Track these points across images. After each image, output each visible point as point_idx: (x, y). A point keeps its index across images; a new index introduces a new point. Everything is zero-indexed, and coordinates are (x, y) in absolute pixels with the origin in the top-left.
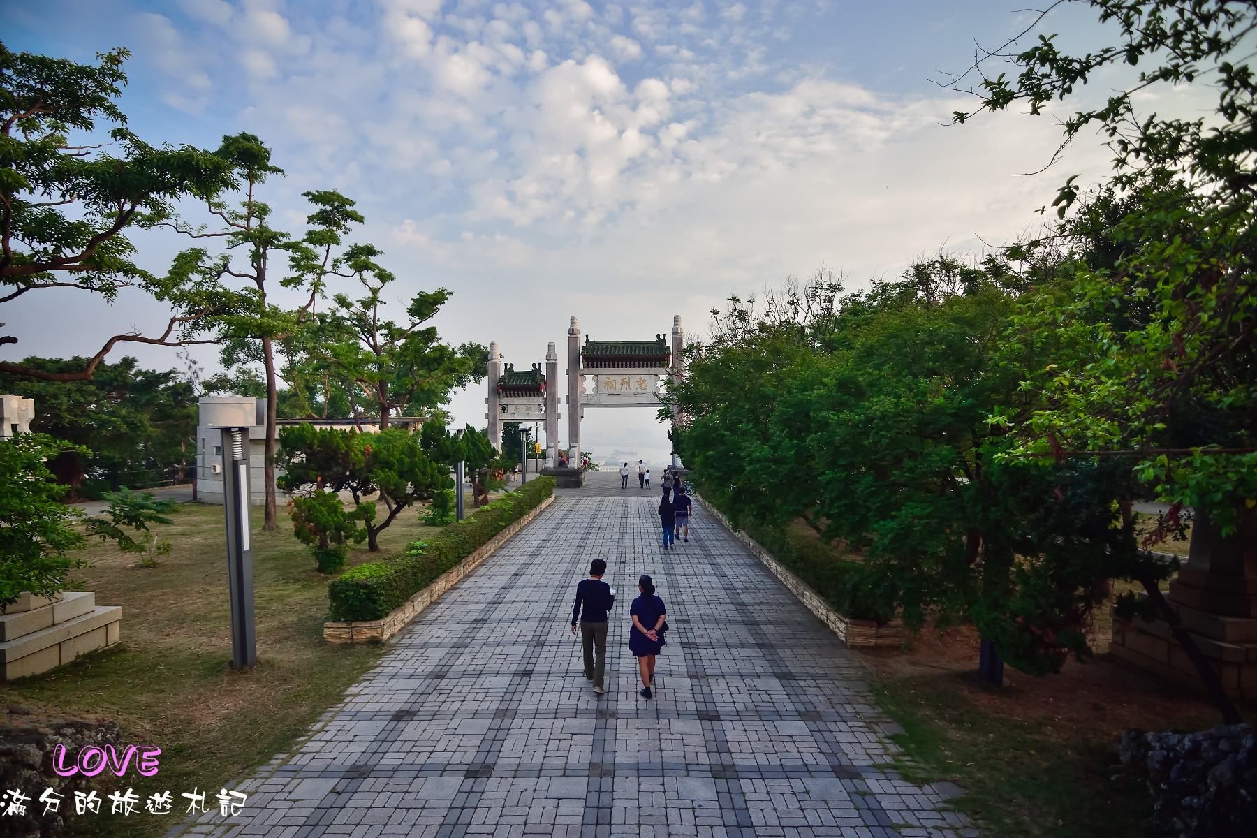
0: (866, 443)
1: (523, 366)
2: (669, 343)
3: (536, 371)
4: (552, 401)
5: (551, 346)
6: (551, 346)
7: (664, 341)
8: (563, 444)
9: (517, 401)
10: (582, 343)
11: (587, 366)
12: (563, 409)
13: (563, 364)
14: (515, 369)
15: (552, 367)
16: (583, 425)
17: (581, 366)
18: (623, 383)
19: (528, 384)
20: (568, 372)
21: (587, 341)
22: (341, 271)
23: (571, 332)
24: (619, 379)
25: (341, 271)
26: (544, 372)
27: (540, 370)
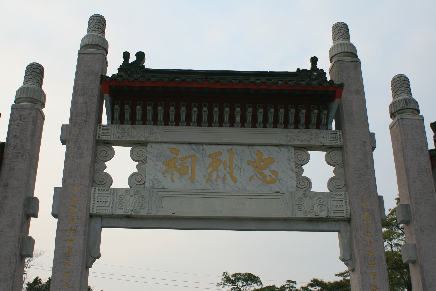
5: (35, 73)
6: (35, 73)
12: (43, 229)
13: (58, 109)
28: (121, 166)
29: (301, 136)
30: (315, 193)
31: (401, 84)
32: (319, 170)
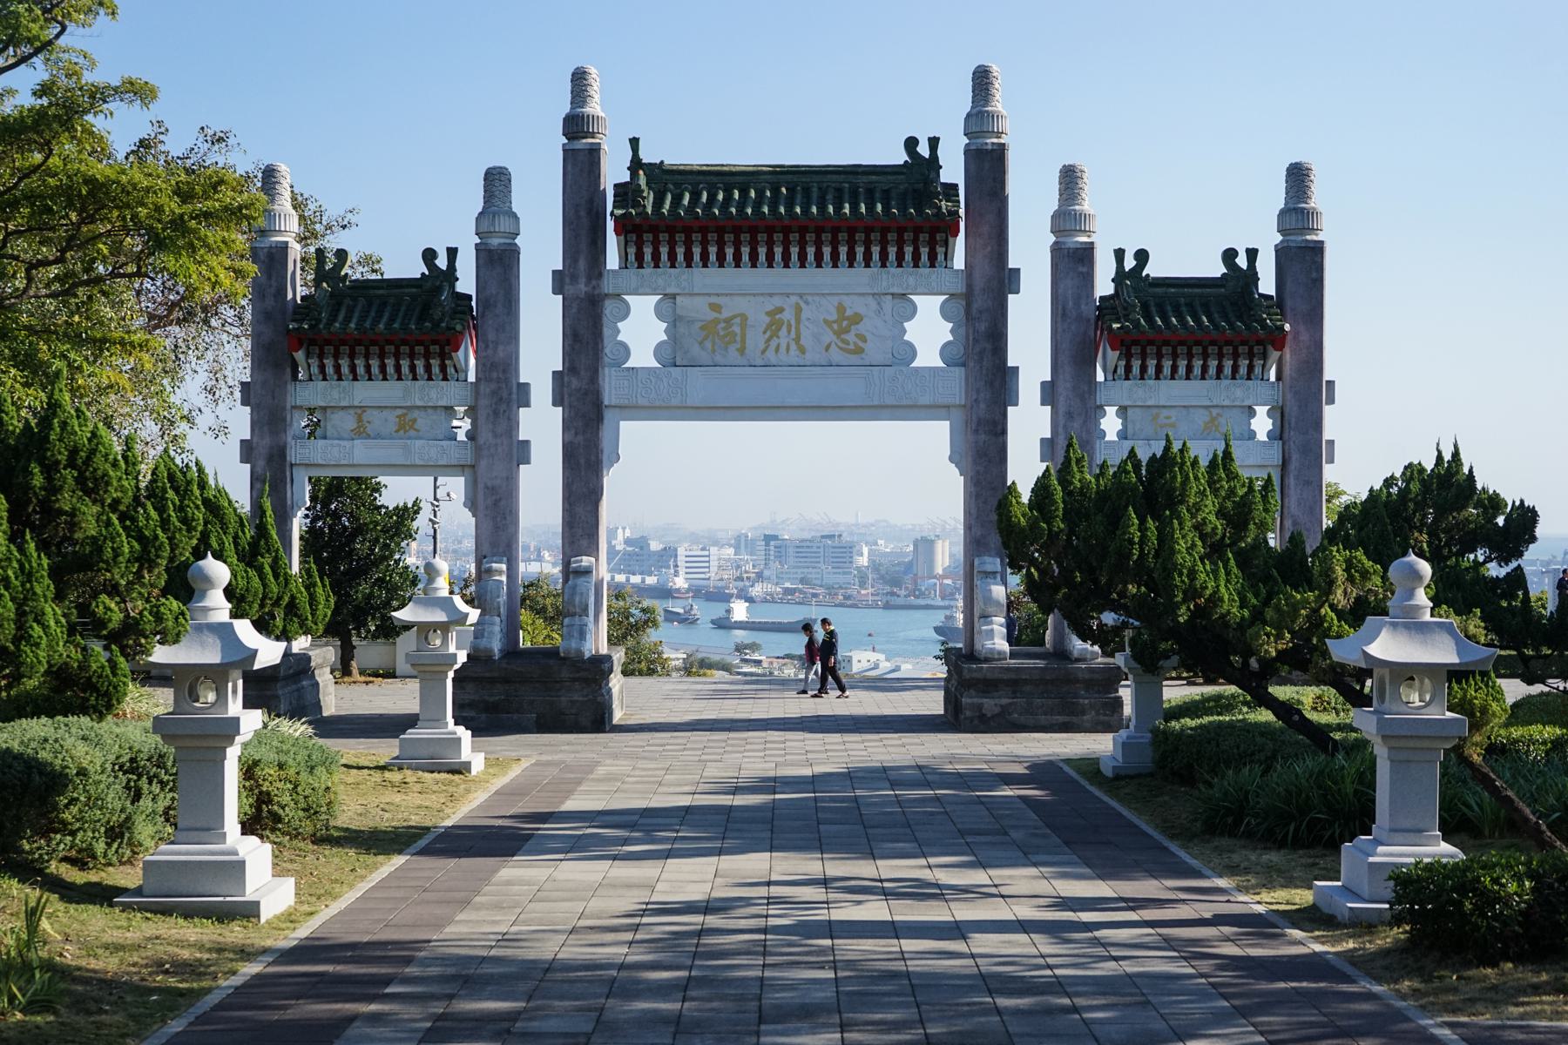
0: (301, 291)
1: (1188, 257)
2: (953, 170)
3: (438, 278)
4: (502, 394)
5: (497, 182)
6: (497, 182)
7: (933, 163)
8: (540, 562)
9: (366, 392)
10: (614, 171)
11: (635, 259)
12: (542, 425)
13: (541, 247)
14: (1153, 270)
15: (499, 261)
16: (613, 481)
17: (613, 260)
18: (774, 327)
19: (386, 327)
20: (560, 281)
21: (636, 164)
22: (392, 416)
23: (576, 126)
24: (757, 313)
25: (392, 416)
26: (466, 283)
27: (450, 275)
28: (640, 330)
29: (892, 278)
30: (917, 369)
31: (1070, 179)
32: (929, 330)
